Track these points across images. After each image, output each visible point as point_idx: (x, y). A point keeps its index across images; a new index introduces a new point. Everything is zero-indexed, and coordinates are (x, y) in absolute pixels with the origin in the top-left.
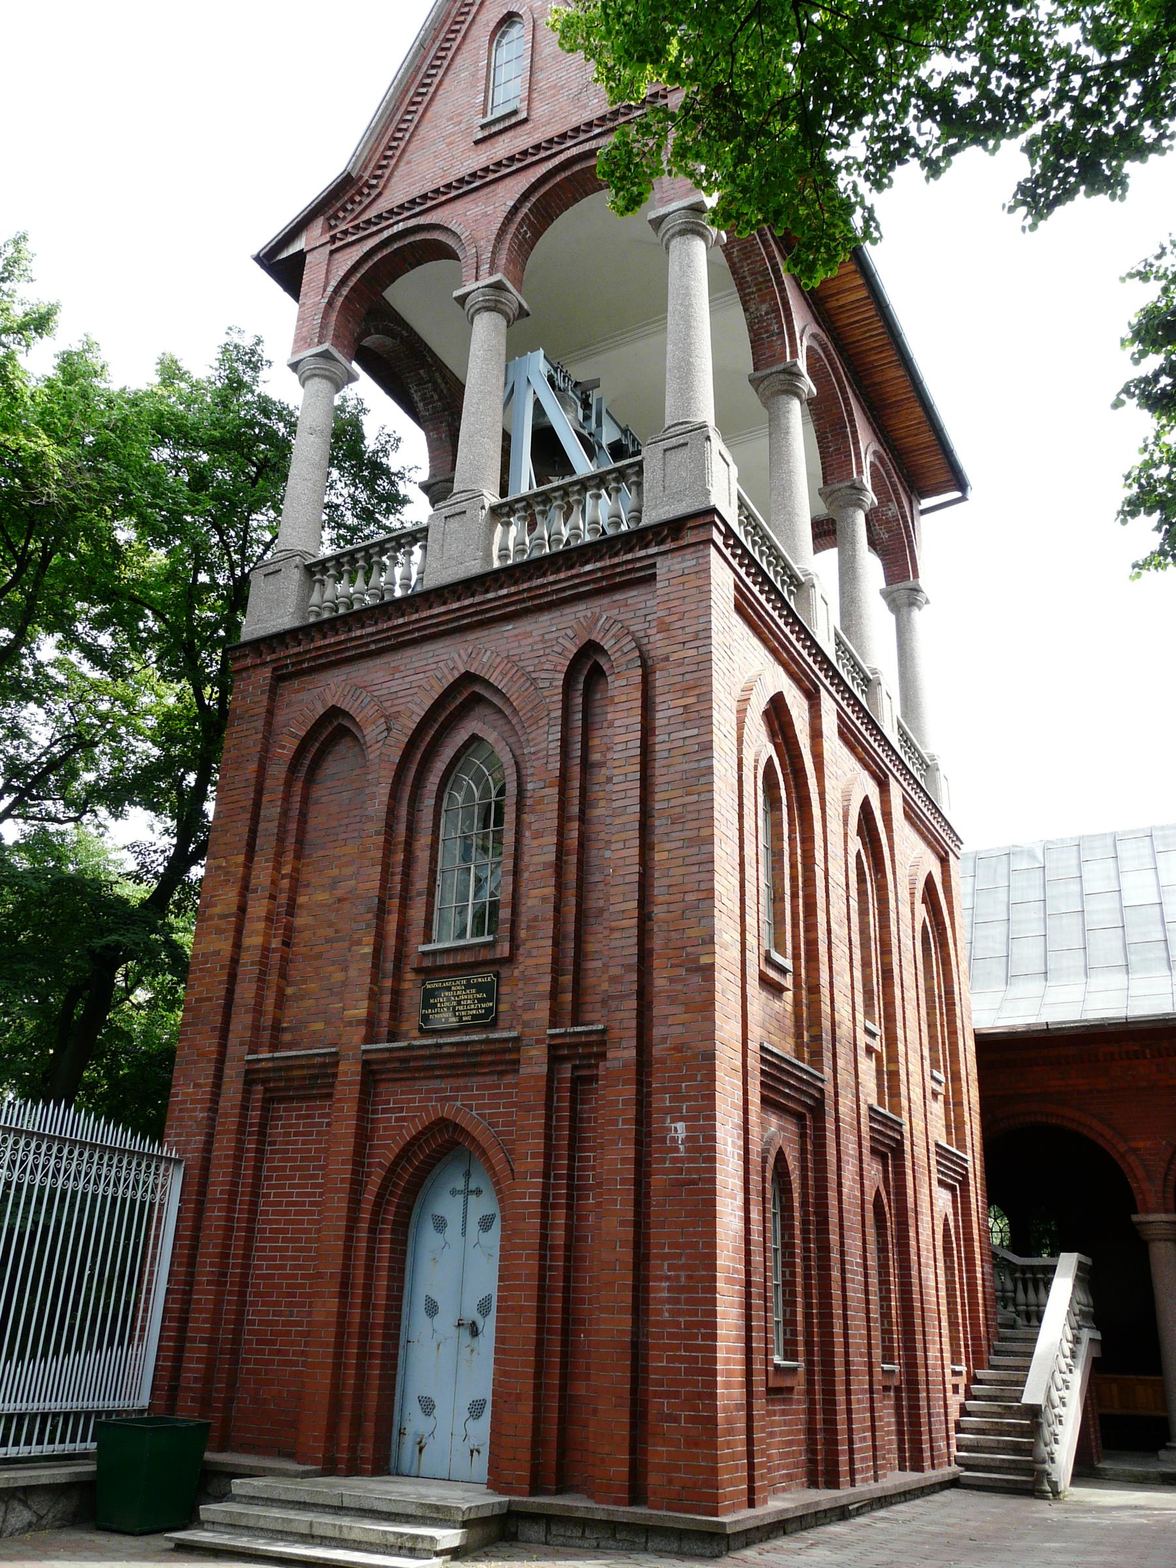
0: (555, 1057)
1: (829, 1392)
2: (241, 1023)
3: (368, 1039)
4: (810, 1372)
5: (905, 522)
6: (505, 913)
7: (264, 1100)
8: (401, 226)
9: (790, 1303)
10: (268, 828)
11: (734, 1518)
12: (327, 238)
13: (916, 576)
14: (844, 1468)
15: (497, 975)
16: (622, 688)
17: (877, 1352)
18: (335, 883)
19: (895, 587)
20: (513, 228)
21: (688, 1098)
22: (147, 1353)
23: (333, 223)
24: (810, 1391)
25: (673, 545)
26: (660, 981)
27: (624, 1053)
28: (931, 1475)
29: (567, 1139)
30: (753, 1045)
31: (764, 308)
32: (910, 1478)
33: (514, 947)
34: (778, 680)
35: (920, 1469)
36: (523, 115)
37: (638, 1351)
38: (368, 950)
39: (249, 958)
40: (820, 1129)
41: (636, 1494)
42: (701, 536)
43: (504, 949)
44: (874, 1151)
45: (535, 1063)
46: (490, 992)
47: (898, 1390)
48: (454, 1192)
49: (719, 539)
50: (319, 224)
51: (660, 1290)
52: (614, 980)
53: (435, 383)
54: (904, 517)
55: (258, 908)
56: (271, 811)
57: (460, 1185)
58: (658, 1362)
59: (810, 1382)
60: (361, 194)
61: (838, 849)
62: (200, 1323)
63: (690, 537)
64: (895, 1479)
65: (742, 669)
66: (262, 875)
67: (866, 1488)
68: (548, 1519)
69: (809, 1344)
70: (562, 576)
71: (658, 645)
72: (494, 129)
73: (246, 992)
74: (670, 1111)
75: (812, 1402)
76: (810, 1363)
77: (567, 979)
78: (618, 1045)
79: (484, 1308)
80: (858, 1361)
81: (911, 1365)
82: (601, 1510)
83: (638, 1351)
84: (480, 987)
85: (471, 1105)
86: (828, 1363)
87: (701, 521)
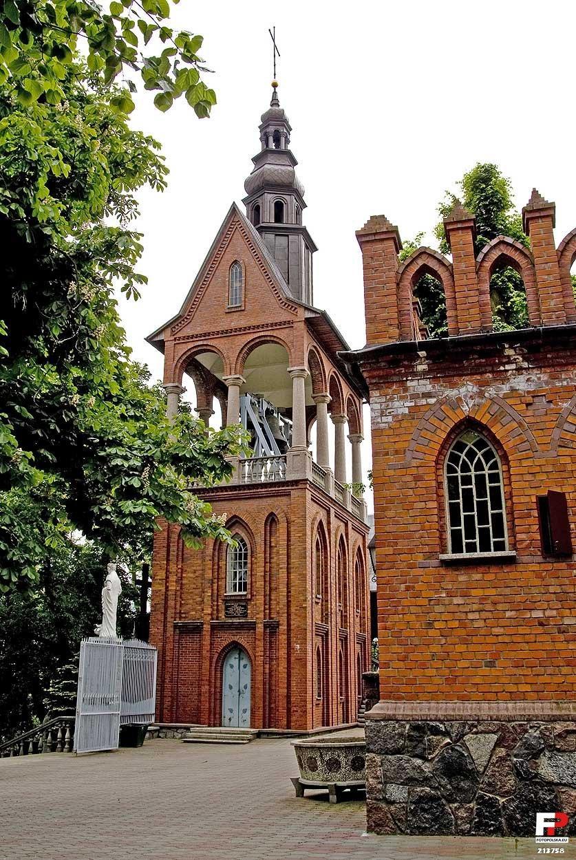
0: (265, 627)
1: (328, 704)
2: (170, 612)
3: (212, 619)
4: (323, 700)
5: (358, 413)
6: (249, 586)
7: (180, 633)
8: (201, 343)
9: (319, 684)
10: (173, 553)
11: (310, 731)
12: (173, 338)
13: (360, 432)
14: (331, 722)
15: (247, 603)
16: (282, 527)
17: (357, 693)
18: (195, 572)
19: (352, 435)
20: (241, 356)
21: (300, 639)
22: (153, 700)
23: (173, 330)
24: (323, 704)
25: (296, 487)
26: (293, 610)
27: (283, 628)
28: (351, 724)
29: (271, 646)
30: (314, 623)
31: (317, 373)
32: (346, 725)
33: (252, 596)
34: (322, 515)
35: (348, 723)
36: (243, 308)
37: (288, 697)
38: (210, 594)
39: (171, 597)
40: (327, 639)
41: (289, 727)
42: (303, 486)
43: (249, 597)
44: (340, 639)
45: (260, 628)
46: (245, 607)
47: (343, 703)
48: (235, 658)
49: (308, 487)
50: (169, 331)
51: (293, 684)
52: (281, 609)
53: (202, 375)
54: (357, 410)
55: (173, 578)
56: (173, 548)
57: (237, 656)
58: (293, 699)
59: (323, 702)
60: (183, 320)
61: (334, 550)
62: (167, 693)
63: (300, 486)
64: (341, 725)
65: (313, 510)
66: (173, 568)
67: (335, 726)
68: (268, 734)
69: (323, 693)
70: (263, 490)
71: (293, 518)
72: (233, 310)
73: (171, 603)
74: (295, 642)
75: (324, 707)
76: (323, 698)
77: (267, 607)
78: (282, 625)
79: (246, 687)
80: (335, 697)
81: (347, 697)
82: (280, 730)
83: (288, 697)
84: (242, 606)
85: (242, 639)
86: (328, 698)
87: (304, 482)
